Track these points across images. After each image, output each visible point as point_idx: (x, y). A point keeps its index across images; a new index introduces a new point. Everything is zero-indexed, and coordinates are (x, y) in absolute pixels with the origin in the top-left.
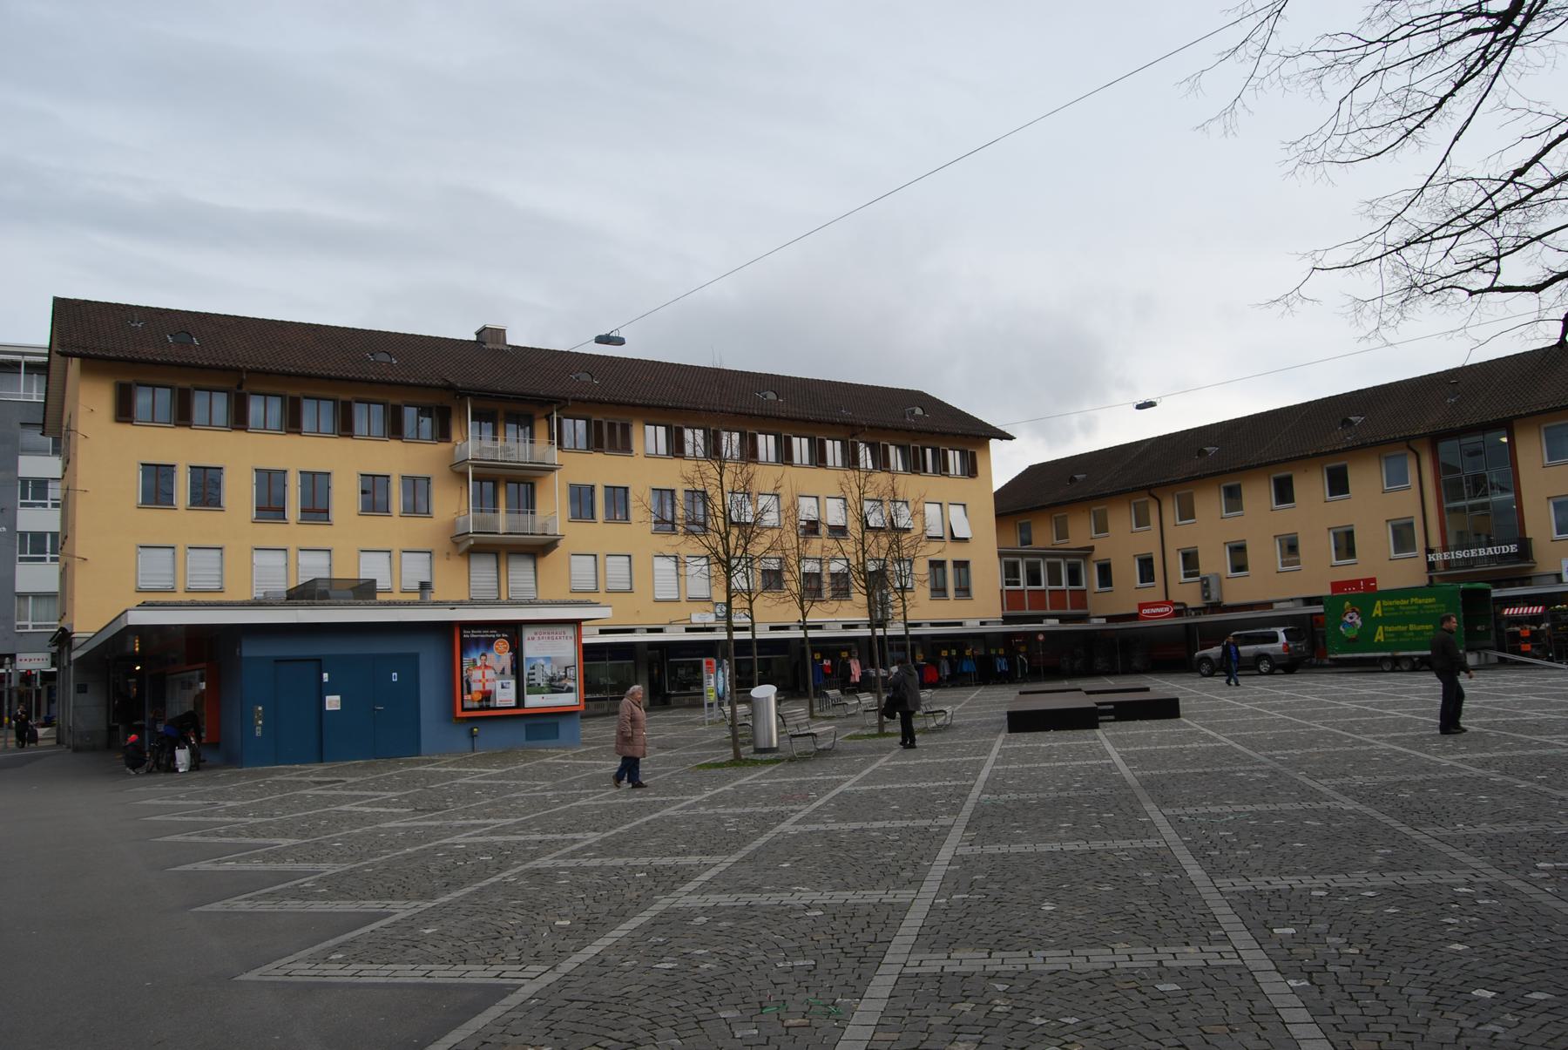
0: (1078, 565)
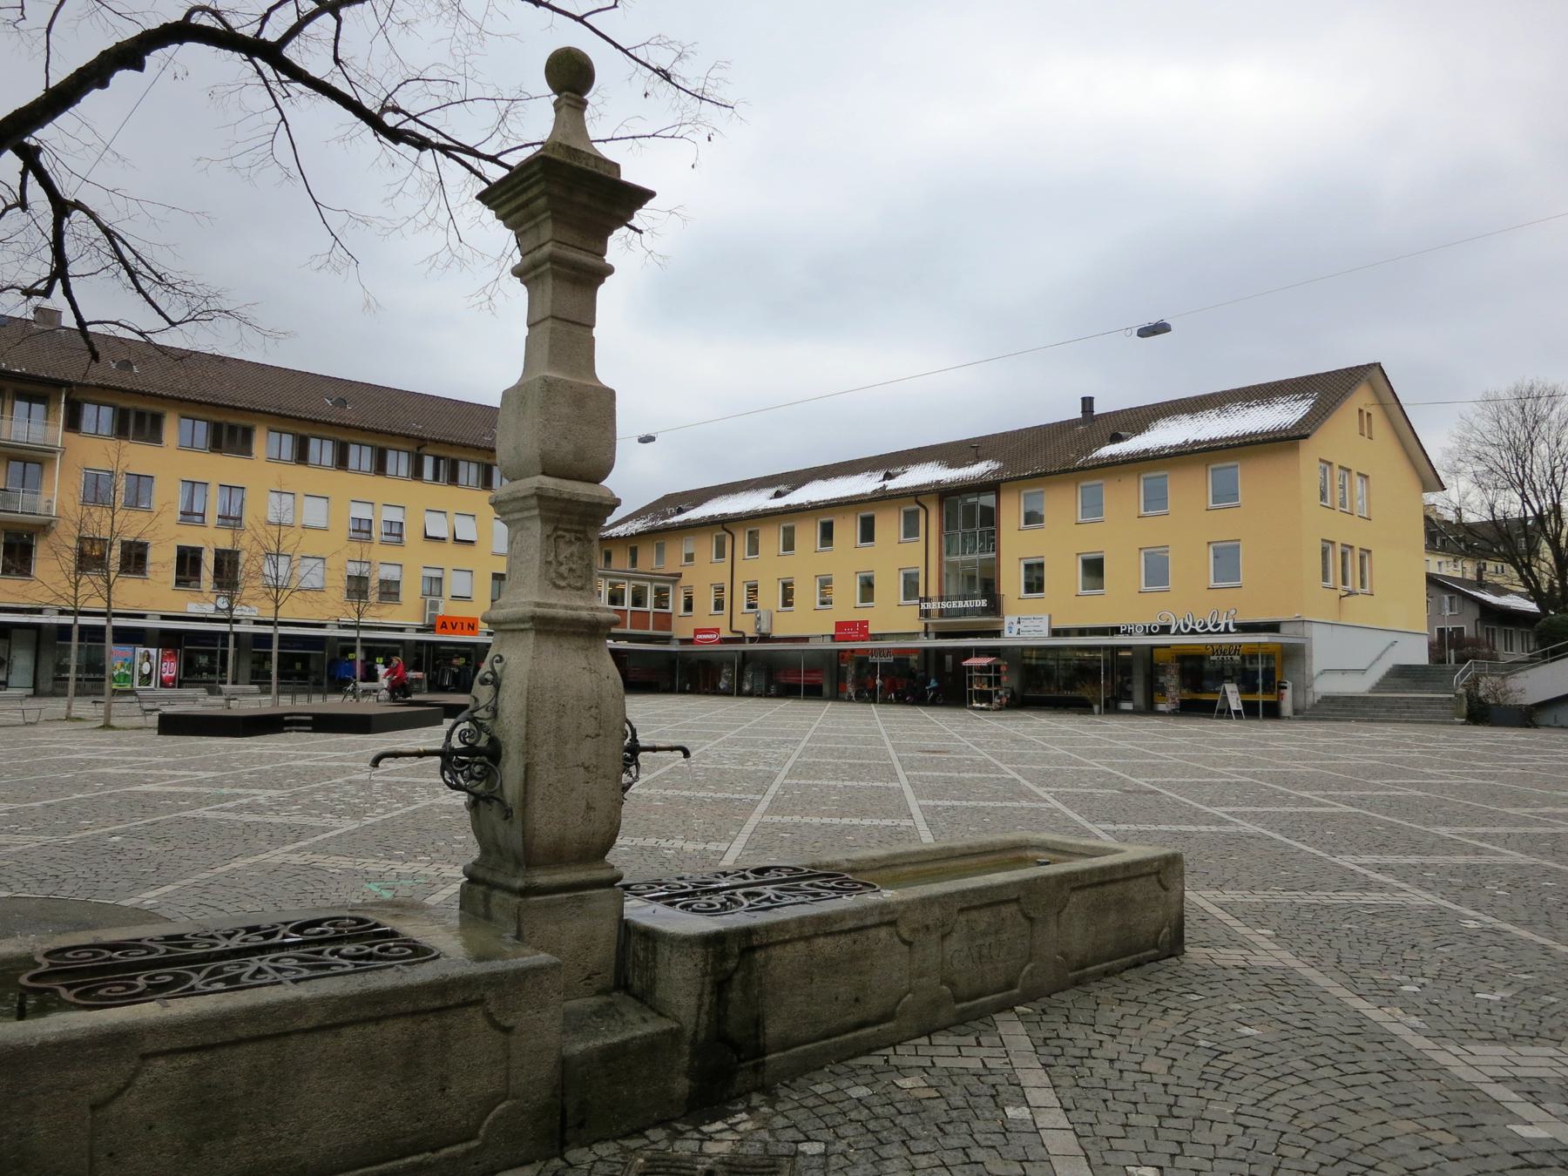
0: (667, 590)
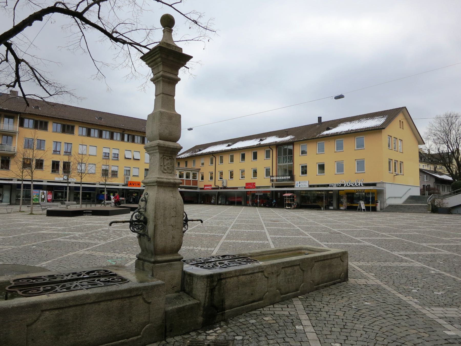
0: (196, 174)
